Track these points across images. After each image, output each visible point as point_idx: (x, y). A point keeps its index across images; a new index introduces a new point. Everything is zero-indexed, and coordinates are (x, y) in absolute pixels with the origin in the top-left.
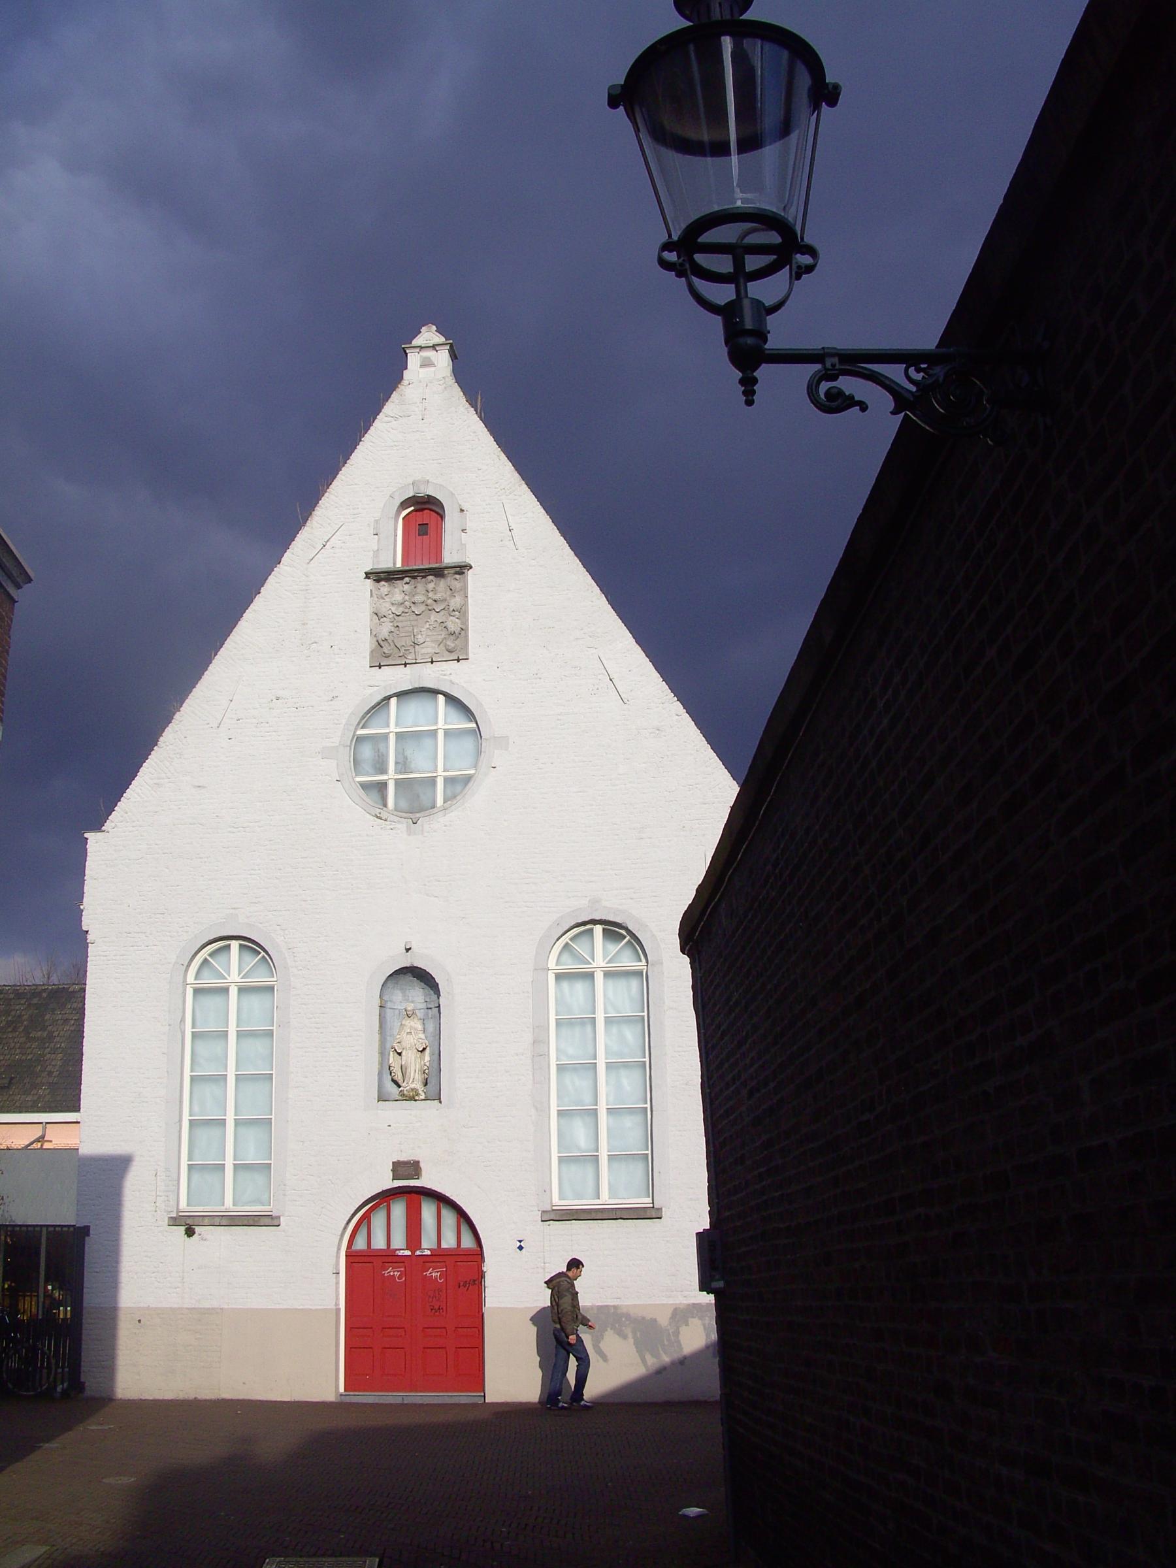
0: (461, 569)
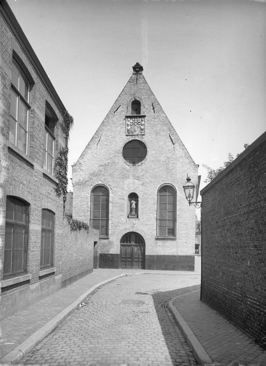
0: (144, 116)
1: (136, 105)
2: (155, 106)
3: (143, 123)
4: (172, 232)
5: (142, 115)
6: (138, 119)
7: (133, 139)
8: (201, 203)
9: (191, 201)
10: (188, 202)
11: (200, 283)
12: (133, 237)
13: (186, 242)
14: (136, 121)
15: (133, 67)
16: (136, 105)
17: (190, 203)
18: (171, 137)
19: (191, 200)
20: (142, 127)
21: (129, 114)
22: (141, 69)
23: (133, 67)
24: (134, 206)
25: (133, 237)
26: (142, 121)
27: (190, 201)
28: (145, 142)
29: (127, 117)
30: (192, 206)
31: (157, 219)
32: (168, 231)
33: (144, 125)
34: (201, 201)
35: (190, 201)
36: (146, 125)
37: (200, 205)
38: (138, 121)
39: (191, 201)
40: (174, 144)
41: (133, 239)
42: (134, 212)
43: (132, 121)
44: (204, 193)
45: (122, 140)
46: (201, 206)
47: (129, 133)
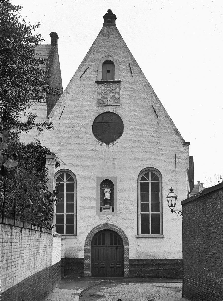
0: (120, 82)
1: (108, 65)
2: (133, 66)
3: (118, 90)
4: (157, 230)
5: (116, 79)
6: (111, 85)
7: (106, 110)
8: (182, 212)
9: (173, 210)
10: (171, 210)
11: (80, 257)
12: (108, 238)
13: (175, 242)
14: (108, 88)
15: (103, 16)
16: (108, 65)
17: (172, 211)
18: (154, 107)
19: (173, 209)
20: (117, 96)
21: (100, 79)
22: (114, 17)
23: (103, 16)
24: (107, 196)
25: (108, 238)
26: (117, 87)
27: (172, 209)
28: (121, 115)
29: (97, 82)
30: (174, 214)
31: (138, 213)
32: (151, 225)
33: (119, 92)
34: (182, 210)
35: (172, 209)
36: (121, 93)
37: (181, 213)
38: (111, 88)
39: (173, 210)
40: (158, 117)
41: (107, 239)
42: (107, 203)
43: (103, 88)
44: (184, 203)
45: (91, 113)
46: (182, 214)
47: (100, 104)
